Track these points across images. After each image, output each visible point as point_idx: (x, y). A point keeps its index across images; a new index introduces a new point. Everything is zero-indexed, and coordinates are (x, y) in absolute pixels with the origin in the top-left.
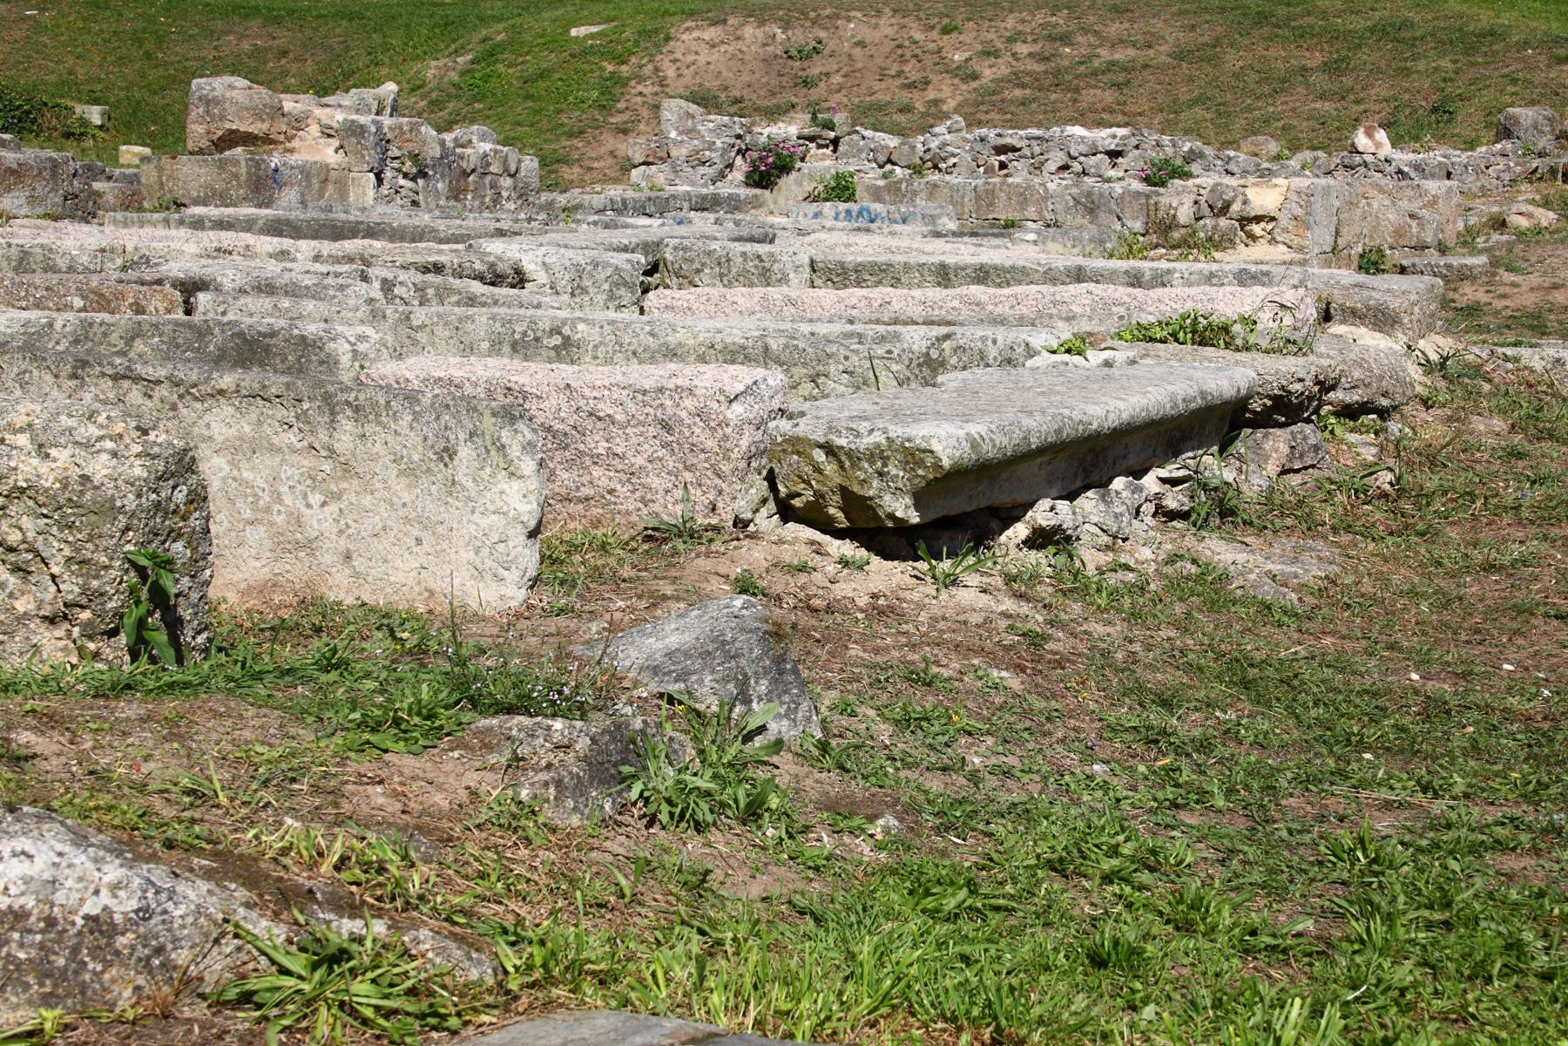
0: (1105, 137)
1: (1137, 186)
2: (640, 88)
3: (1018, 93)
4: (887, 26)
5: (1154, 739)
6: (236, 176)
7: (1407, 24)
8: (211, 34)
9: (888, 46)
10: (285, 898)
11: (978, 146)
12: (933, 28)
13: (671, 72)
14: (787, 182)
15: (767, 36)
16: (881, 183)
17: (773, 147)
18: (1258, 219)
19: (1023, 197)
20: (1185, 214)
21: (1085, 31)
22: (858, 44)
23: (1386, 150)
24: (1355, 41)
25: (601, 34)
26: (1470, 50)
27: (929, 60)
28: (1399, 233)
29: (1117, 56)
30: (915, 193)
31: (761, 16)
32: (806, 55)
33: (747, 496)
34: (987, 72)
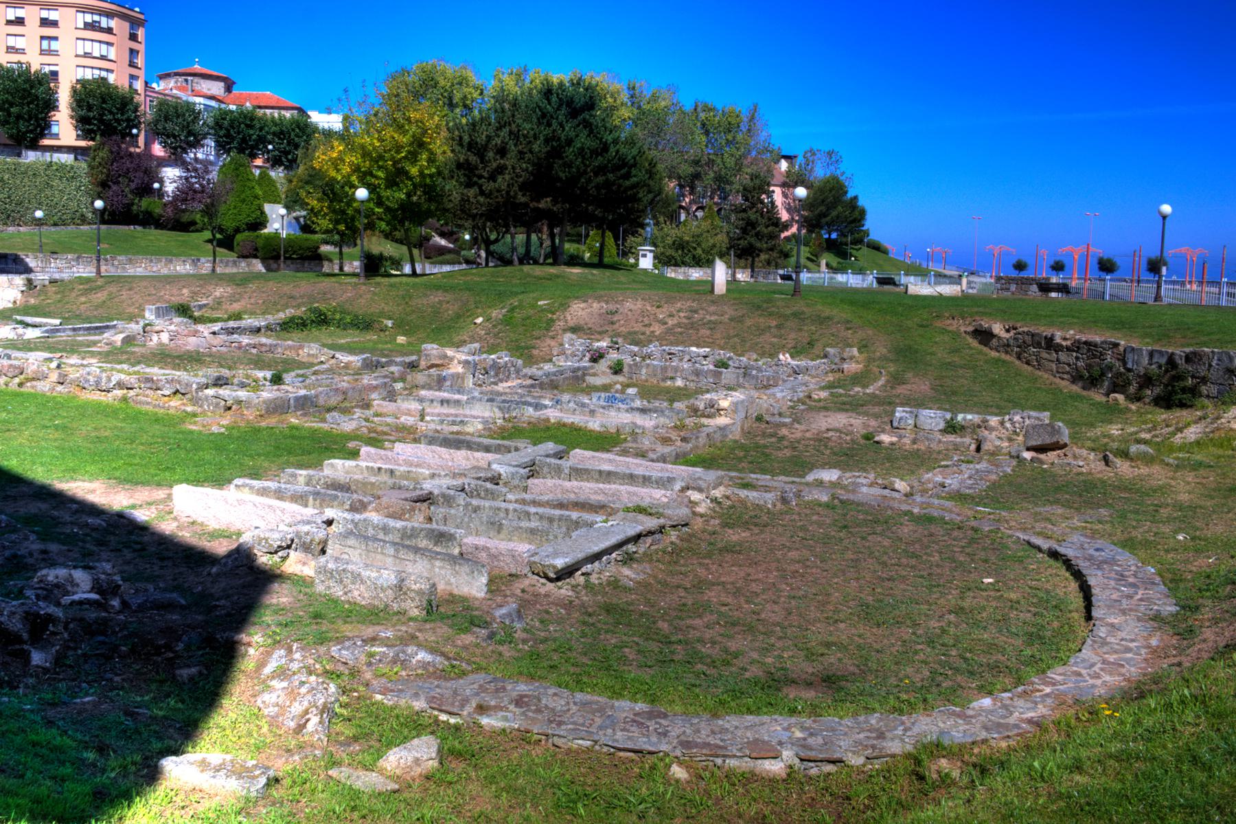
0: (703, 351)
1: (711, 367)
4: (639, 304)
5: (584, 623)
7: (803, 313)
8: (426, 295)
10: (449, 659)
14: (602, 361)
19: (676, 369)
20: (702, 406)
23: (789, 360)
24: (786, 317)
26: (821, 323)
32: (612, 313)
33: (526, 570)
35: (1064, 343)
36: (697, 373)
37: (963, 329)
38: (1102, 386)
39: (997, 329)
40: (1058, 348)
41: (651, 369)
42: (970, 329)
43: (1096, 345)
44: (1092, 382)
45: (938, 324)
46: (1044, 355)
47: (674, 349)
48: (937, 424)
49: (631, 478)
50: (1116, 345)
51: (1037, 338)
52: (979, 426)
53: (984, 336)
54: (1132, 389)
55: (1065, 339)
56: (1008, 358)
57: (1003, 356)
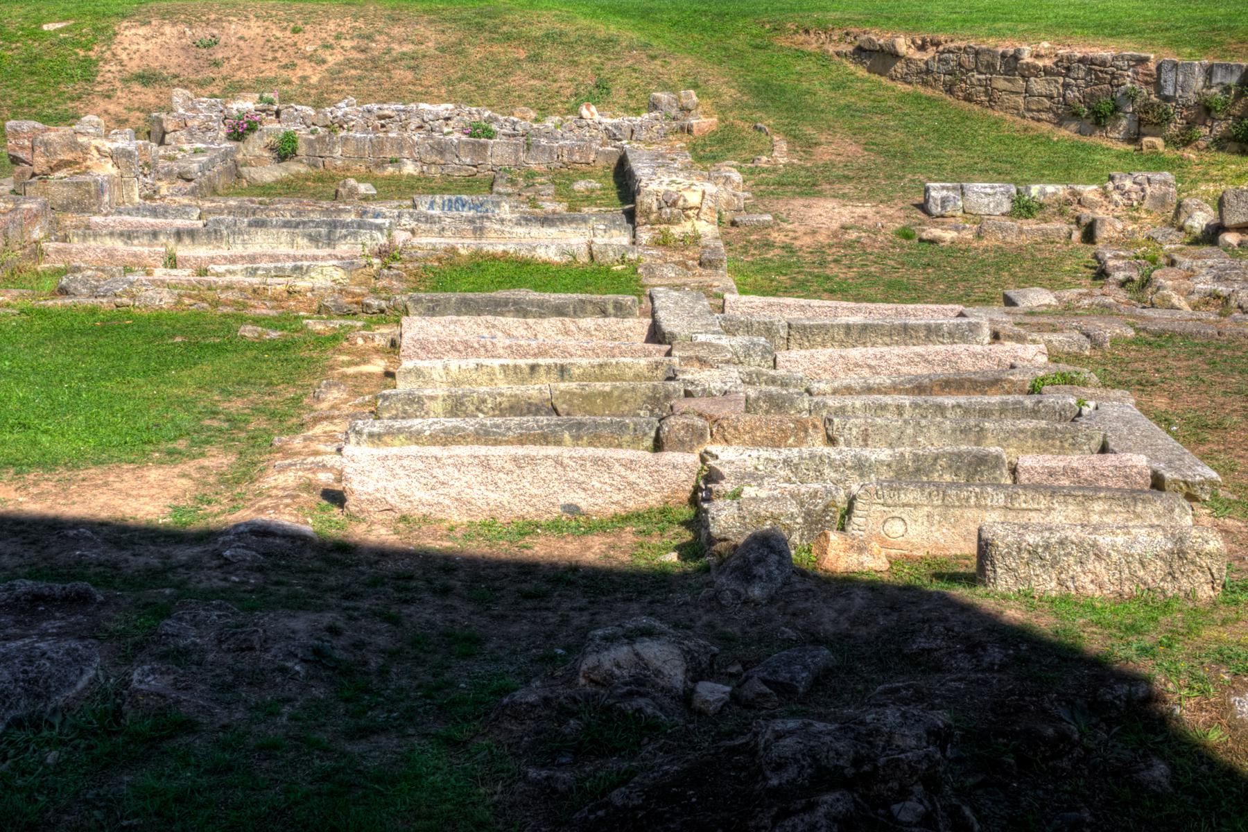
2: (108, 67)
3: (353, 72)
6: (88, 192)
9: (261, 41)
11: (367, 115)
12: (285, 29)
13: (124, 56)
15: (180, 33)
16: (312, 137)
17: (242, 115)
18: (691, 208)
19: (400, 145)
21: (380, 33)
22: (241, 38)
23: (597, 117)
25: (67, 30)
27: (291, 50)
28: (728, 203)
29: (404, 49)
30: (334, 143)
31: (168, 16)
34: (330, 59)
35: (1040, 63)
36: (441, 149)
37: (831, 49)
38: (1114, 127)
39: (902, 45)
40: (1029, 72)
41: (351, 149)
42: (847, 48)
43: (1103, 63)
44: (1099, 119)
45: (782, 41)
46: (1000, 83)
47: (390, 108)
48: (998, 204)
49: (905, 333)
50: (1142, 61)
51: (984, 59)
52: (1068, 203)
53: (879, 58)
54: (1173, 129)
55: (1038, 56)
56: (929, 92)
57: (921, 90)
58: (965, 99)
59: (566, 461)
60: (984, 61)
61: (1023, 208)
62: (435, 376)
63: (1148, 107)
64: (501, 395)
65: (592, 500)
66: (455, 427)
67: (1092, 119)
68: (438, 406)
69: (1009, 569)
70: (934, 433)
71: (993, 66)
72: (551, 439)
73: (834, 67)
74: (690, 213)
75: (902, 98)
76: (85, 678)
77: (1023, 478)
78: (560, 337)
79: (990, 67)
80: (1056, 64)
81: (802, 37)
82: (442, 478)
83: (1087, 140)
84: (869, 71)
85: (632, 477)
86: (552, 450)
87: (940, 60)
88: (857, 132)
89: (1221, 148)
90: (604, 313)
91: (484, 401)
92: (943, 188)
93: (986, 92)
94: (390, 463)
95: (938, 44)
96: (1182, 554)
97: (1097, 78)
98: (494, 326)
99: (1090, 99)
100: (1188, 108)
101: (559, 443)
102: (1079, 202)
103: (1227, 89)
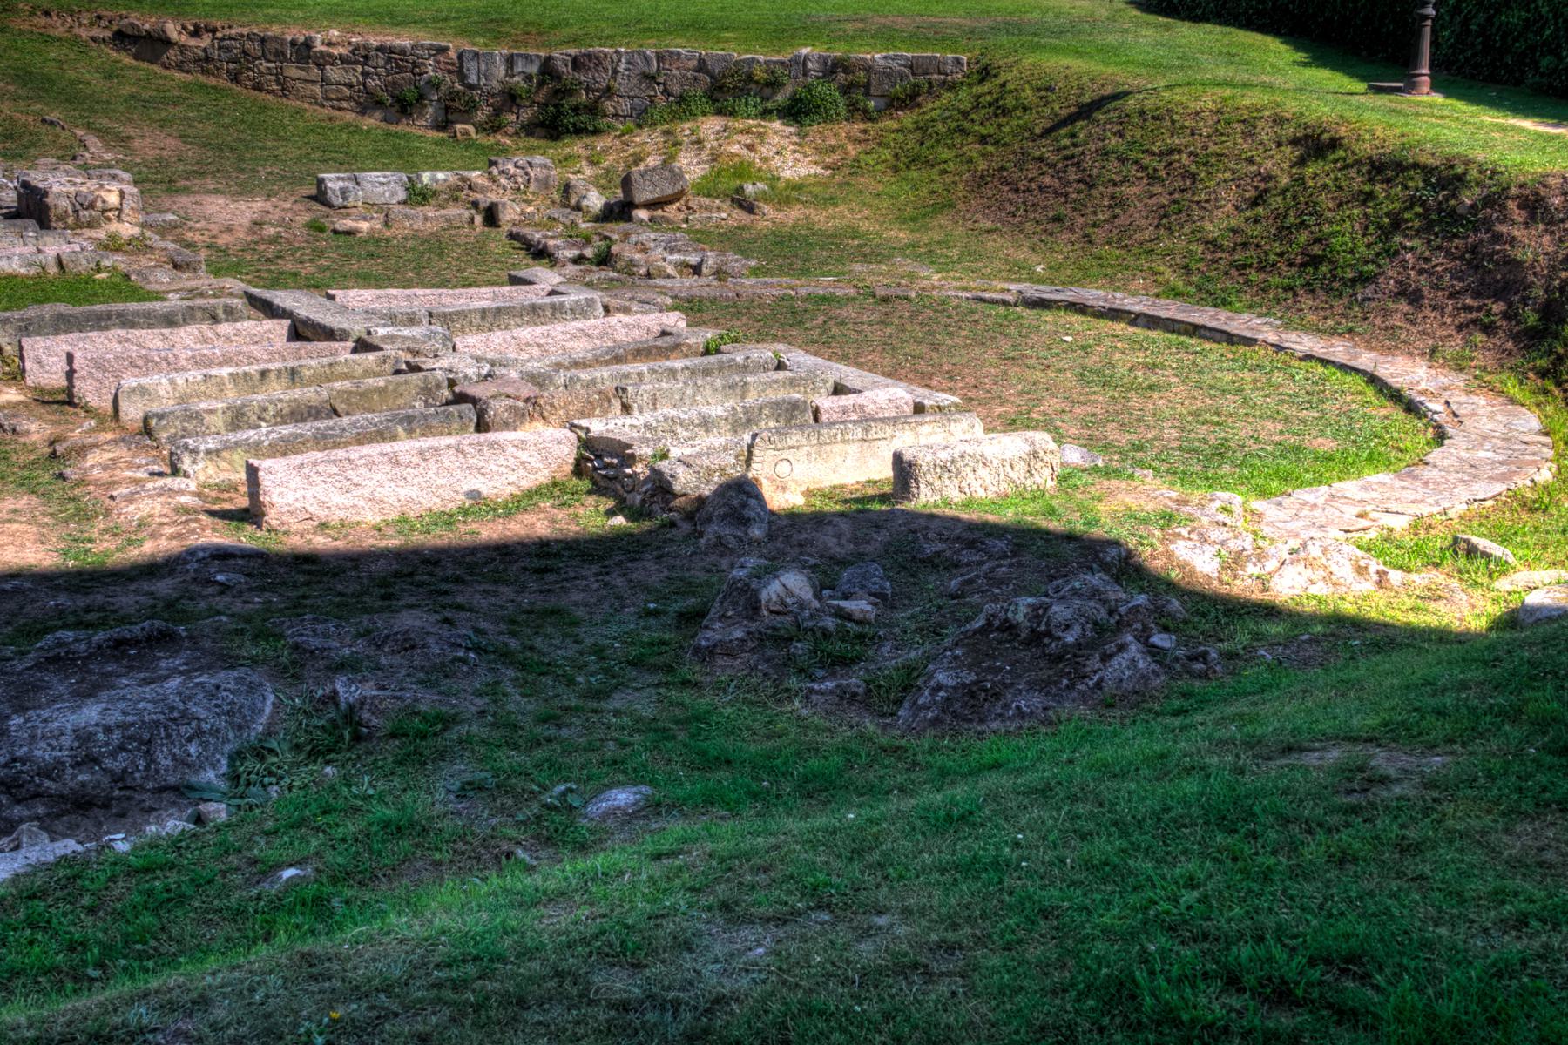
35: (335, 52)
38: (421, 115)
39: (172, 30)
40: (323, 61)
43: (403, 52)
44: (404, 107)
46: (293, 71)
48: (393, 194)
53: (152, 45)
54: (480, 116)
55: (330, 44)
56: (213, 81)
57: (202, 78)
58: (254, 88)
59: (467, 448)
60: (271, 48)
61: (418, 196)
62: (162, 393)
63: (453, 95)
64: (281, 401)
65: (491, 484)
66: (292, 434)
67: (397, 107)
68: (217, 421)
69: (928, 484)
70: (708, 392)
71: (284, 54)
72: (387, 435)
73: (94, 54)
74: (110, 214)
75: (187, 87)
76: (269, 703)
77: (824, 418)
78: (199, 346)
79: (280, 55)
80: (352, 52)
81: (43, 20)
82: (356, 480)
83: (400, 128)
84: (136, 58)
85: (524, 456)
86: (387, 447)
87: (220, 48)
88: (163, 124)
89: (530, 134)
90: (214, 319)
91: (265, 409)
92: (339, 179)
93: (278, 82)
94: (306, 470)
95: (214, 31)
96: (1035, 454)
97: (398, 66)
98: (127, 340)
99: (392, 87)
100: (493, 96)
101: (394, 438)
102: (470, 187)
103: (529, 78)
